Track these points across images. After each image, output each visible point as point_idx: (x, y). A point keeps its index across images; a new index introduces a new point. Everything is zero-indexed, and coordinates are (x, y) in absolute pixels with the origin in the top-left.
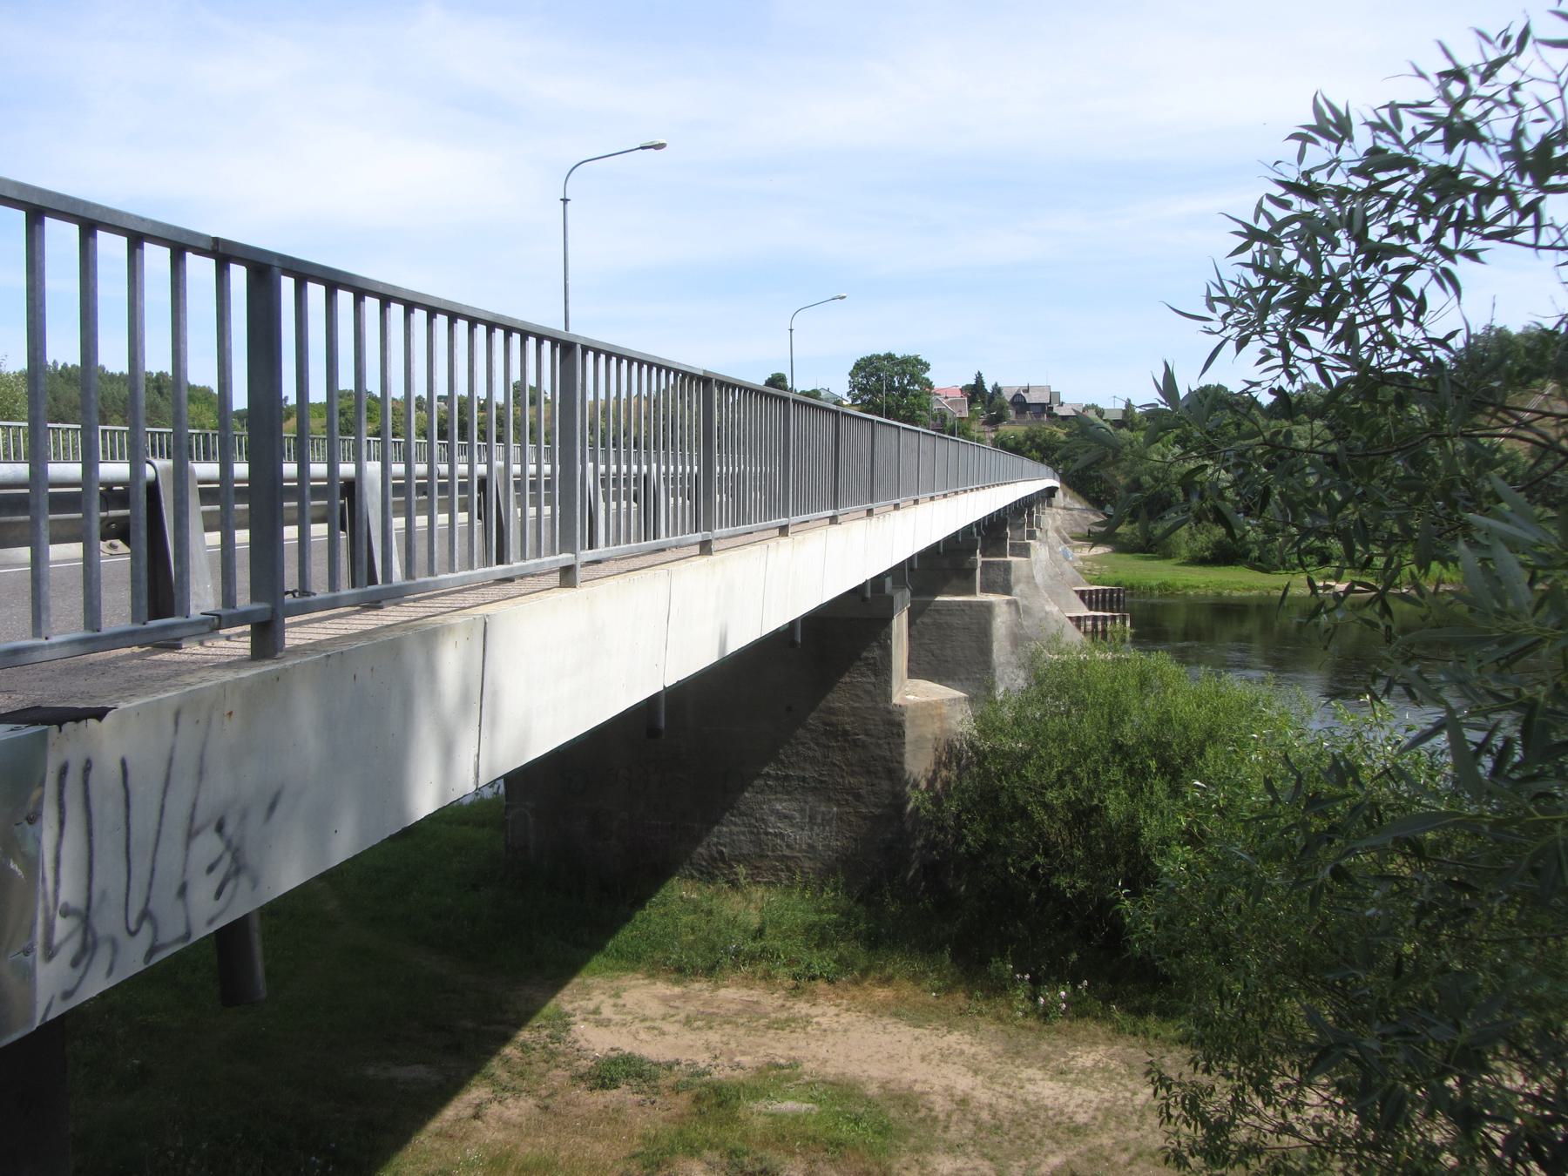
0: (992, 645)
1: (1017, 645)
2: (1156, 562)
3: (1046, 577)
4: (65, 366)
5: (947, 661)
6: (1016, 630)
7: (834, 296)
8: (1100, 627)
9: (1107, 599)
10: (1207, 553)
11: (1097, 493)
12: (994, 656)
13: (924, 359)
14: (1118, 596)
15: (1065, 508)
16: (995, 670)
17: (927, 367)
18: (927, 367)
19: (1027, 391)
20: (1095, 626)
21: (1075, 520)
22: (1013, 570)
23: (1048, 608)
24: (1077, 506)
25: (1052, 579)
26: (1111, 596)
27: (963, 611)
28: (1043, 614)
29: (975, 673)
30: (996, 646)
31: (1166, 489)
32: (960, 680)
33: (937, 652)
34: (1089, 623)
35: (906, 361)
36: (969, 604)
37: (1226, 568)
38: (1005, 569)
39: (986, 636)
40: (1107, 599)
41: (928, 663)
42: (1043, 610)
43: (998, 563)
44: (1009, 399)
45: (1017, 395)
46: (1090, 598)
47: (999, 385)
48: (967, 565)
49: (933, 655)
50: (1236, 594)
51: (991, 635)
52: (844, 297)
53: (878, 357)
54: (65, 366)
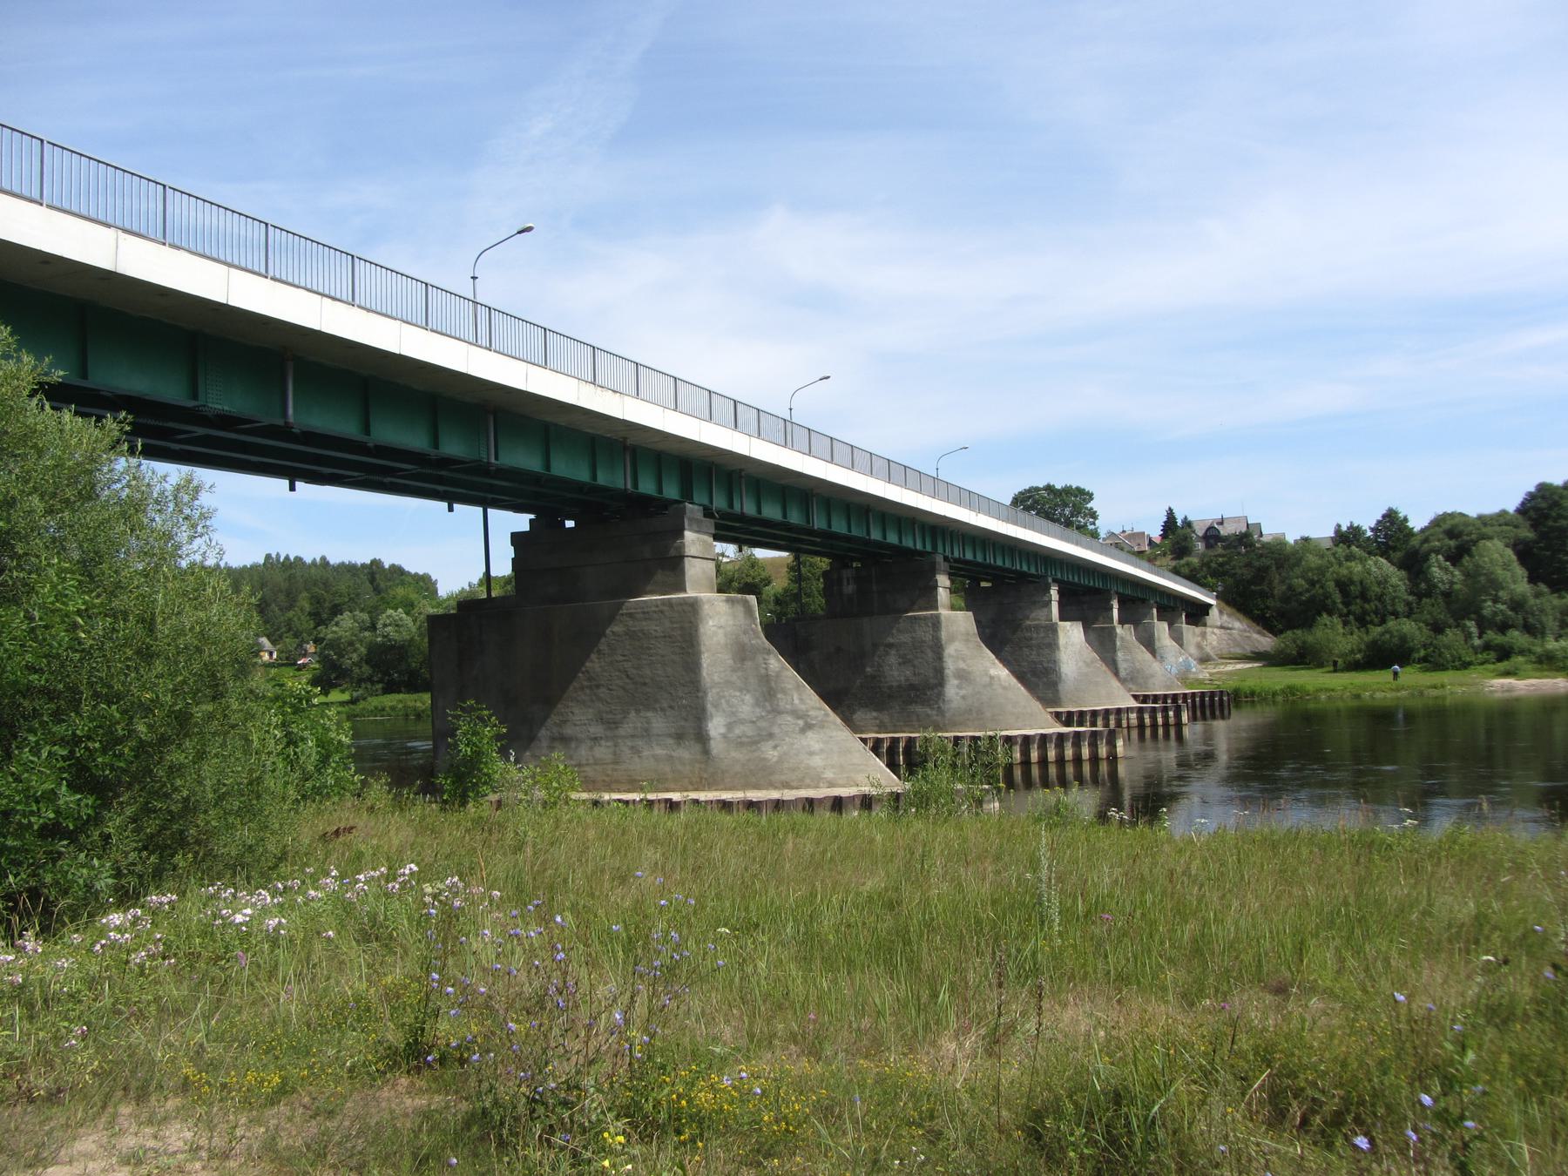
0: (699, 658)
1: (743, 660)
2: (1303, 671)
3: (1081, 664)
4: (287, 558)
5: (645, 684)
6: (745, 639)
7: (520, 228)
8: (1160, 720)
9: (1198, 703)
10: (1358, 656)
11: (1262, 610)
12: (704, 673)
13: (1087, 488)
14: (1221, 700)
15: (1222, 627)
16: (705, 693)
17: (1090, 496)
18: (1090, 496)
19: (1221, 523)
20: (1141, 719)
21: (1234, 640)
22: (944, 624)
23: (993, 672)
24: (1237, 625)
25: (1088, 665)
26: (1202, 701)
27: (662, 612)
28: (988, 679)
29: (682, 698)
30: (706, 660)
31: (1321, 591)
32: (663, 710)
33: (632, 672)
34: (1133, 716)
35: (1067, 491)
36: (669, 603)
37: (1382, 672)
38: (934, 624)
39: (693, 646)
40: (1198, 703)
41: (624, 689)
42: (986, 673)
43: (925, 618)
44: (1201, 533)
45: (1211, 528)
46: (1194, 701)
47: (1190, 518)
48: (672, 553)
49: (628, 676)
50: (1378, 695)
51: (699, 644)
52: (529, 229)
53: (1037, 489)
54: (287, 558)
